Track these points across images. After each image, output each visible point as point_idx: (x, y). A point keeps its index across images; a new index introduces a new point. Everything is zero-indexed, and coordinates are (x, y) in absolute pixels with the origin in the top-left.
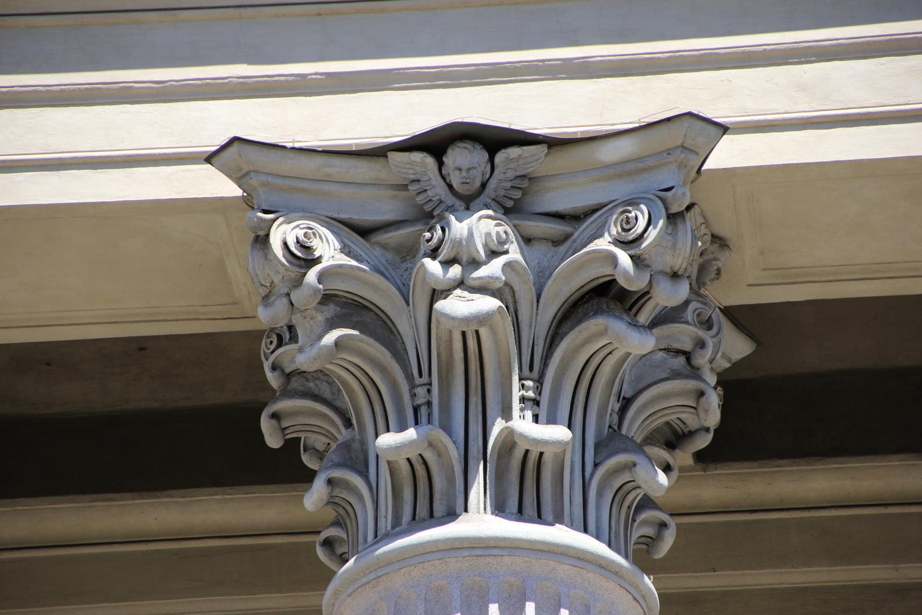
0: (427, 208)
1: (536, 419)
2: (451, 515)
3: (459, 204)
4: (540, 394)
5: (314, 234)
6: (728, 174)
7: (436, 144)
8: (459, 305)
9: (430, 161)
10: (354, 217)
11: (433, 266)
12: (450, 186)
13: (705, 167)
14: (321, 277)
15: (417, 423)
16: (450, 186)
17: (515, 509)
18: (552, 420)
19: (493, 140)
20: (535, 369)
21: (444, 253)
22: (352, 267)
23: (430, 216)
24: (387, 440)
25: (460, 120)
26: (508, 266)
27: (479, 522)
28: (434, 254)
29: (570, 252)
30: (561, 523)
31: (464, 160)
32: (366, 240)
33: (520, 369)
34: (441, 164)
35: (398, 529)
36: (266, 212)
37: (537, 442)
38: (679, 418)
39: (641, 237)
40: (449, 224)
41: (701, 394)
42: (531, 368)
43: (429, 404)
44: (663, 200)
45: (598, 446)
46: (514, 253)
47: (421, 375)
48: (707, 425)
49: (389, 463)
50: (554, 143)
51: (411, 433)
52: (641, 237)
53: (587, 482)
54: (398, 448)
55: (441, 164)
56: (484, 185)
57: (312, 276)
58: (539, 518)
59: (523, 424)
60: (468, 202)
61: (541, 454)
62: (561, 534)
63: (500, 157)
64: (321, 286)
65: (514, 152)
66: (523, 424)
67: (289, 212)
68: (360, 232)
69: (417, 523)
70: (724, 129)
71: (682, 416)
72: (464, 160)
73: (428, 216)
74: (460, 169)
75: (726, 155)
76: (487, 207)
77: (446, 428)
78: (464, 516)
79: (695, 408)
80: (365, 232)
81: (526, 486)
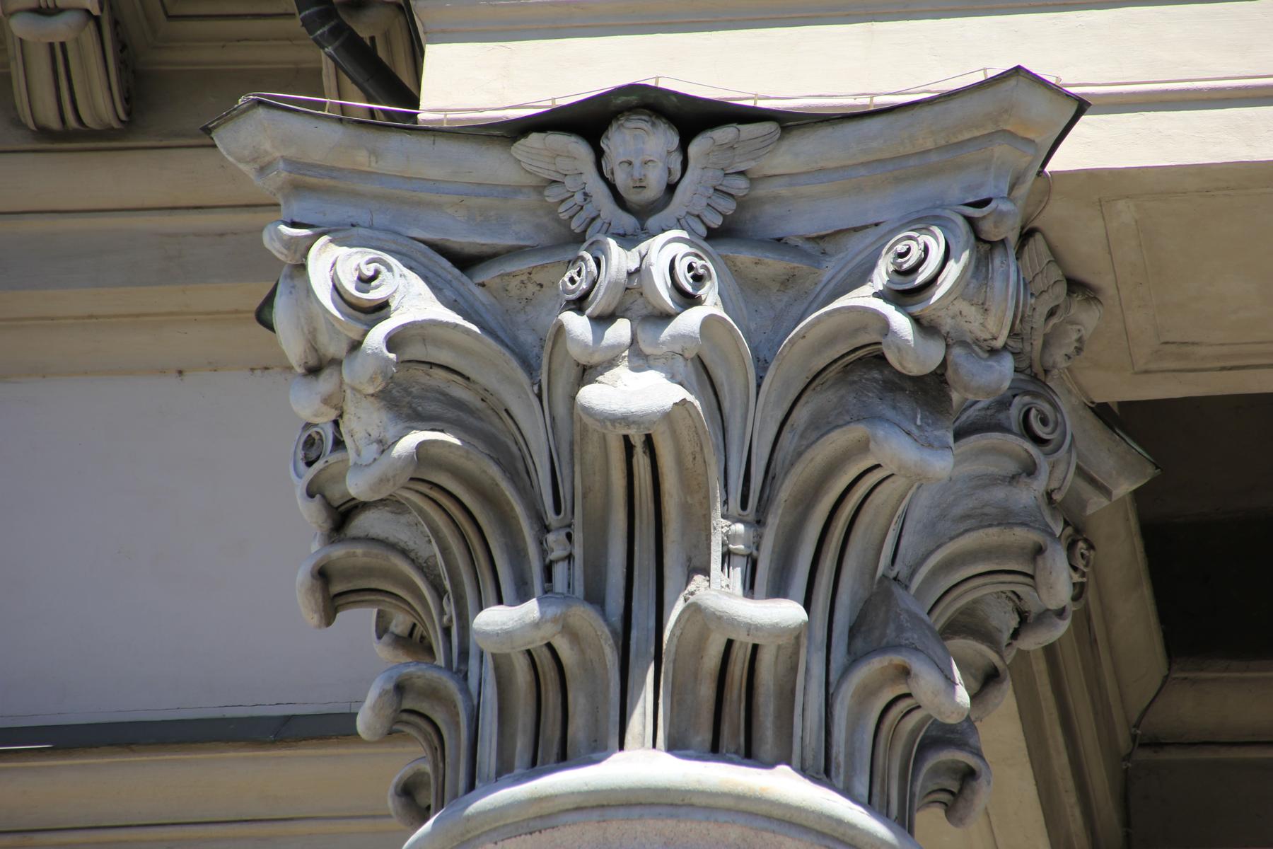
0: (576, 226)
1: (750, 588)
2: (596, 751)
3: (627, 221)
4: (758, 549)
5: (1056, 423)
6: (1102, 186)
7: (589, 121)
8: (634, 392)
9: (577, 148)
10: (452, 239)
11: (577, 325)
12: (612, 187)
13: (1048, 169)
14: (393, 341)
15: (548, 590)
16: (612, 187)
17: (706, 736)
18: (779, 590)
19: (691, 118)
20: (755, 504)
21: (597, 304)
22: (456, 326)
23: (579, 239)
24: (494, 619)
25: (652, 83)
26: (708, 322)
27: (642, 763)
28: (579, 305)
29: (815, 305)
30: (789, 763)
31: (641, 148)
32: (471, 278)
33: (726, 502)
34: (599, 154)
35: (505, 772)
36: (294, 225)
37: (751, 628)
38: (1014, 592)
39: (932, 282)
40: (605, 252)
41: (1039, 551)
42: (744, 505)
43: (570, 558)
44: (970, 221)
45: (853, 632)
46: (711, 304)
47: (558, 510)
48: (1053, 605)
49: (493, 655)
50: (789, 122)
51: (531, 609)
52: (932, 282)
53: (831, 691)
54: (507, 635)
55: (599, 154)
56: (671, 188)
57: (377, 337)
58: (749, 755)
59: (721, 593)
60: (640, 217)
61: (755, 648)
62: (784, 784)
63: (697, 147)
64: (392, 356)
65: (725, 134)
66: (721, 593)
67: (343, 233)
68: (457, 264)
69: (536, 766)
70: (1082, 106)
71: (1018, 589)
72: (641, 148)
73: (572, 239)
74: (630, 163)
75: (1087, 148)
76: (679, 225)
77: (595, 597)
78: (618, 756)
79: (1032, 577)
80: (466, 262)
81: (733, 708)
